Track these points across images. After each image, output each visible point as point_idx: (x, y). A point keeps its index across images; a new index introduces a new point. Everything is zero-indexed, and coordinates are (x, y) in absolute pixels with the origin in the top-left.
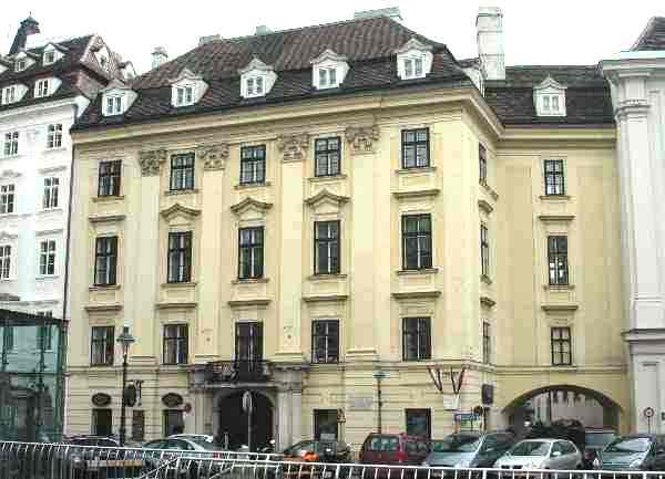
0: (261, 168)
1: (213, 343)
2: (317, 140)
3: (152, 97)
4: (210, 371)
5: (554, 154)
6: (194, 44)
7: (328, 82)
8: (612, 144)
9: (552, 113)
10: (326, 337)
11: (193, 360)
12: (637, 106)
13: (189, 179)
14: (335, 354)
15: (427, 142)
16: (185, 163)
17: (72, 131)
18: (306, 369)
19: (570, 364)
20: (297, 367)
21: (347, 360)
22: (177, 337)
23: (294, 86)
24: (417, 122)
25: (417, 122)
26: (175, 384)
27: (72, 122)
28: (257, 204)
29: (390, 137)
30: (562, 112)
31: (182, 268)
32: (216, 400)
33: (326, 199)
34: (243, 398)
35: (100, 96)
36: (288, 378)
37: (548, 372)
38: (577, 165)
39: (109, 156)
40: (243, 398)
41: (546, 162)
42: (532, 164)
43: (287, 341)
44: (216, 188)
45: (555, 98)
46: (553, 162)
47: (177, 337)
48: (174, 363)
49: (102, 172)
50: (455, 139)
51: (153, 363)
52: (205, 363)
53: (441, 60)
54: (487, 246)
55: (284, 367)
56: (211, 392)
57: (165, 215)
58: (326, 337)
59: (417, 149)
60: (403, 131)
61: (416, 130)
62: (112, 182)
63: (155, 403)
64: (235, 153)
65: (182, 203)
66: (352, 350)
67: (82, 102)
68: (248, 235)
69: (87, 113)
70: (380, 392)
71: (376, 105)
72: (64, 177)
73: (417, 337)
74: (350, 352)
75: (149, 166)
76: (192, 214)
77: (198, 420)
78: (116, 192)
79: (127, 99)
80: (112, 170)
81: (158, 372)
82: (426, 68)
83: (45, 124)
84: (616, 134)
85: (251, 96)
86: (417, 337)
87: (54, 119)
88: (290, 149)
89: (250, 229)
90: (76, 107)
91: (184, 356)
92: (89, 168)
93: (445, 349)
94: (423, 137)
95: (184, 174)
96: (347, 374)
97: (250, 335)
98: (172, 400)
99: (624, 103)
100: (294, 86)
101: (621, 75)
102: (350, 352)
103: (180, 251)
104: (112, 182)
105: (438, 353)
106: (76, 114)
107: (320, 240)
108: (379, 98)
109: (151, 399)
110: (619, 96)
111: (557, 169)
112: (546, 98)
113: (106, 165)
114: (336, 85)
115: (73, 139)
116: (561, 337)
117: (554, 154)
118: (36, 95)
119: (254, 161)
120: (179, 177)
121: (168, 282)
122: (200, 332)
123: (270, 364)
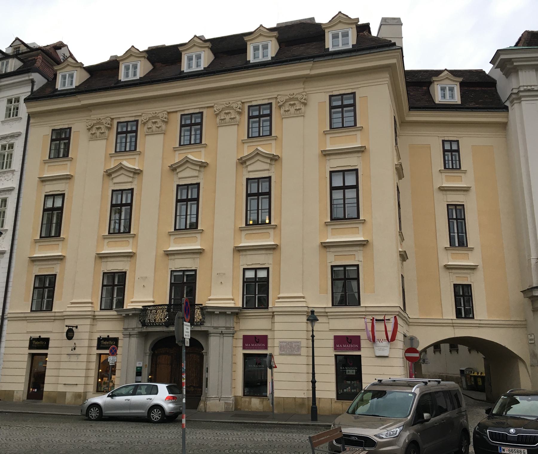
0: (133, 139)
1: (147, 291)
2: (118, 123)
3: (104, 76)
4: (143, 313)
5: (451, 135)
6: (146, 49)
8: (504, 126)
9: (448, 100)
10: (257, 292)
11: (128, 305)
12: (529, 90)
13: (133, 144)
14: (264, 303)
15: (354, 105)
16: (193, 122)
17: (26, 100)
18: (236, 314)
20: (229, 312)
22: (115, 285)
26: (110, 328)
27: (30, 94)
28: (129, 170)
30: (457, 99)
31: (54, 225)
32: (150, 342)
34: (173, 344)
35: (55, 75)
36: (221, 322)
37: (453, 325)
38: (470, 143)
39: (61, 123)
40: (173, 344)
41: (443, 141)
42: (432, 142)
43: (220, 291)
44: (156, 151)
45: (451, 89)
46: (451, 142)
47: (115, 285)
48: (111, 309)
49: (54, 137)
50: (377, 102)
51: (90, 309)
52: (141, 307)
56: (144, 336)
57: (109, 174)
58: (257, 292)
59: (343, 108)
60: (331, 96)
61: (342, 95)
63: (90, 347)
64: (176, 120)
65: (125, 163)
66: (281, 295)
67: (40, 80)
68: (120, 196)
69: (42, 89)
70: (313, 336)
73: (345, 286)
74: (279, 298)
75: (95, 132)
76: (135, 173)
77: (130, 356)
78: (66, 154)
81: (94, 318)
82: (352, 40)
83: (480, 326)
84: (507, 117)
86: (345, 286)
87: (12, 93)
88: (223, 118)
90: (33, 82)
91: (121, 303)
92: (42, 134)
93: (379, 293)
94: (264, 188)
95: (127, 136)
96: (277, 318)
97: (184, 284)
98: (107, 344)
99: (519, 88)
101: (515, 64)
102: (279, 298)
104: (62, 146)
106: (32, 88)
109: (86, 336)
110: (505, 87)
111: (454, 147)
112: (443, 89)
114: (138, 77)
115: (28, 107)
116: (463, 298)
117: (451, 135)
119: (192, 125)
120: (124, 140)
121: (41, 237)
122: (136, 279)
123: (203, 309)
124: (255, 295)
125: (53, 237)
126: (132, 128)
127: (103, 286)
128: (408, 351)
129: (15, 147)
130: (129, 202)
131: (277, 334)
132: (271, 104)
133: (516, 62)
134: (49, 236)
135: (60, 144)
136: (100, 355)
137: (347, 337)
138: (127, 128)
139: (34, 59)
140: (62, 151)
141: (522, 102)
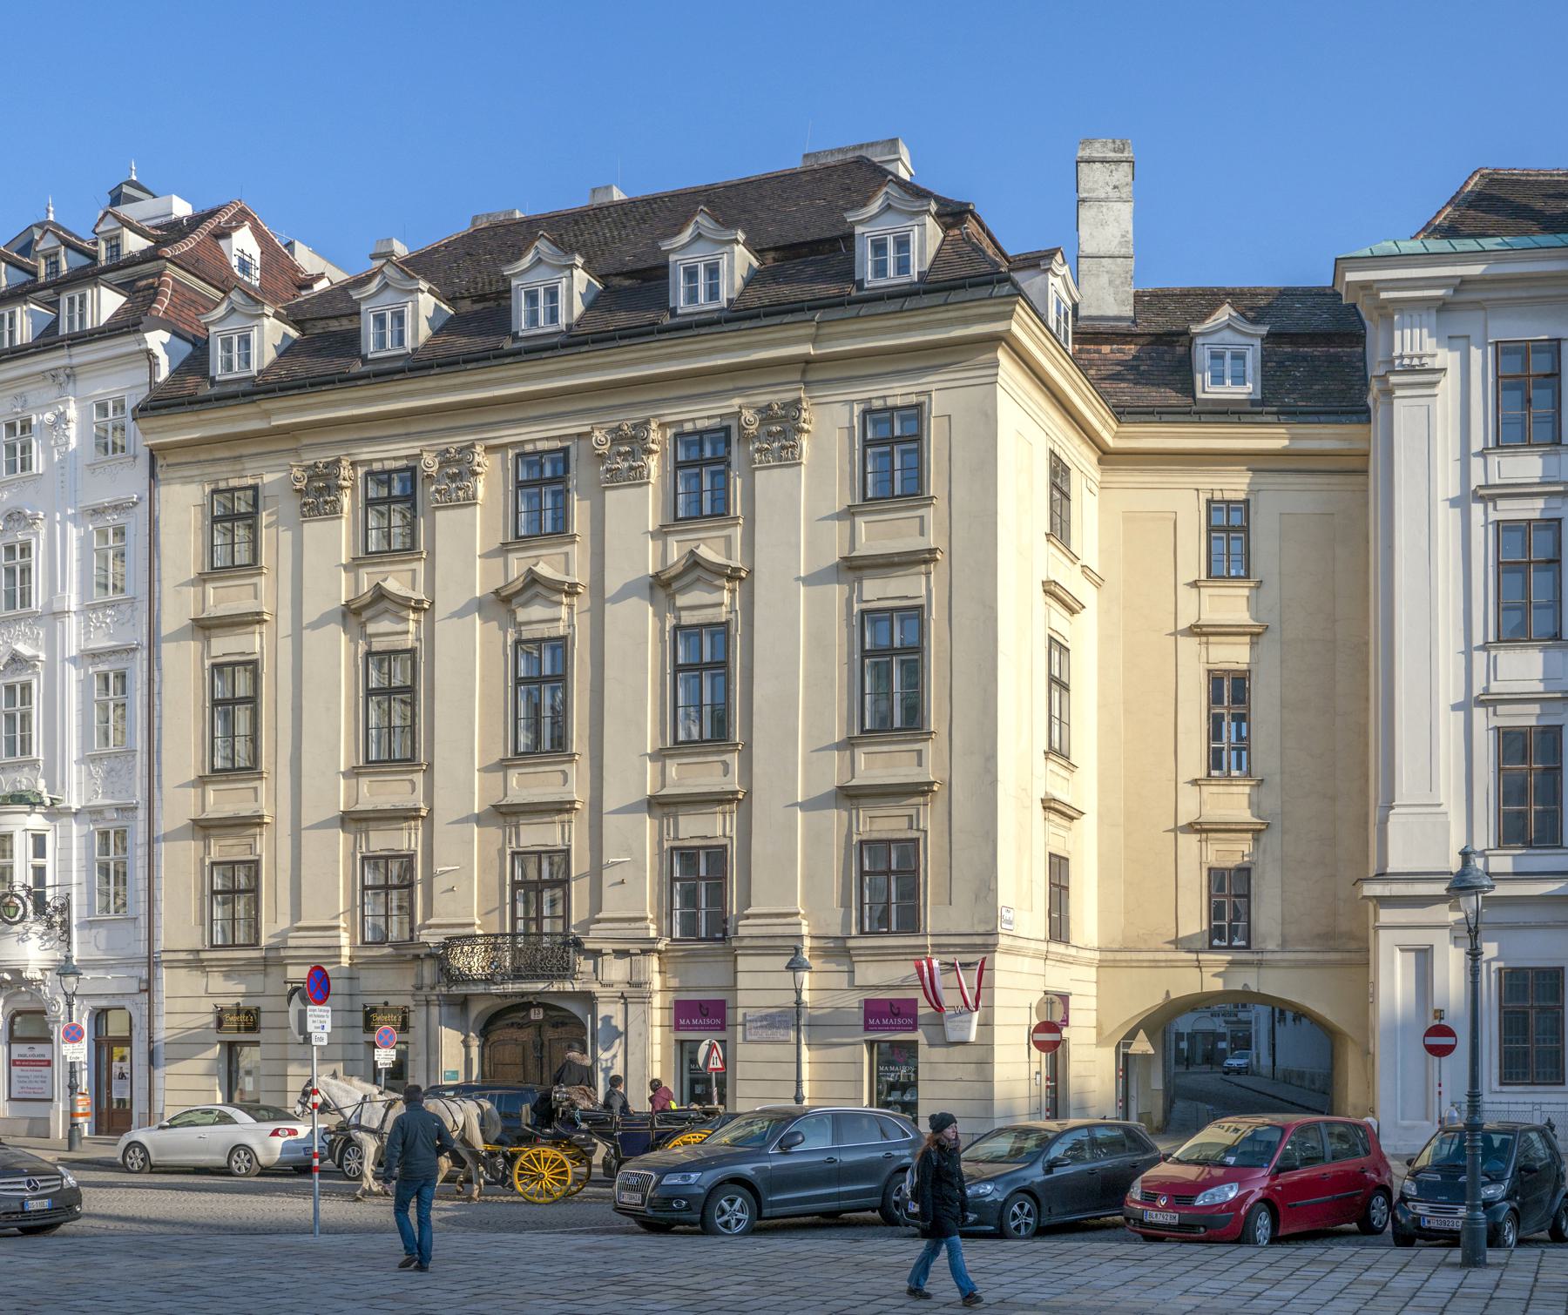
1: (466, 894)
7: (891, 271)
16: (708, 453)
19: (1248, 947)
21: (291, 943)
23: (635, 294)
24: (898, 392)
25: (898, 392)
29: (829, 426)
33: (698, 572)
47: (393, 881)
53: (967, 239)
54: (1065, 687)
55: (607, 947)
62: (707, 485)
66: (299, 924)
68: (884, 625)
71: (809, 349)
72: (136, 524)
79: (270, 335)
80: (708, 453)
85: (882, 282)
89: (539, 642)
90: (150, 355)
92: (183, 504)
100: (635, 294)
101: (1383, 295)
103: (396, 695)
104: (548, 502)
105: (932, 919)
107: (875, 652)
108: (809, 330)
113: (313, 473)
118: (64, 329)
124: (699, 909)
125: (898, 730)
126: (714, 450)
127: (862, 874)
128: (1038, 1029)
129: (130, 533)
130: (912, 640)
131: (743, 998)
132: (727, 429)
133: (1387, 290)
134: (535, 750)
135: (699, 476)
136: (1525, 1041)
137: (700, 1004)
138: (702, 450)
139: (151, 287)
140: (707, 496)
141: (757, 473)
